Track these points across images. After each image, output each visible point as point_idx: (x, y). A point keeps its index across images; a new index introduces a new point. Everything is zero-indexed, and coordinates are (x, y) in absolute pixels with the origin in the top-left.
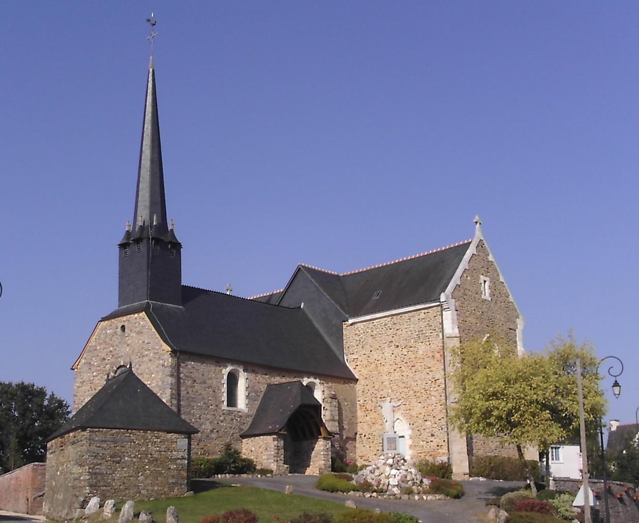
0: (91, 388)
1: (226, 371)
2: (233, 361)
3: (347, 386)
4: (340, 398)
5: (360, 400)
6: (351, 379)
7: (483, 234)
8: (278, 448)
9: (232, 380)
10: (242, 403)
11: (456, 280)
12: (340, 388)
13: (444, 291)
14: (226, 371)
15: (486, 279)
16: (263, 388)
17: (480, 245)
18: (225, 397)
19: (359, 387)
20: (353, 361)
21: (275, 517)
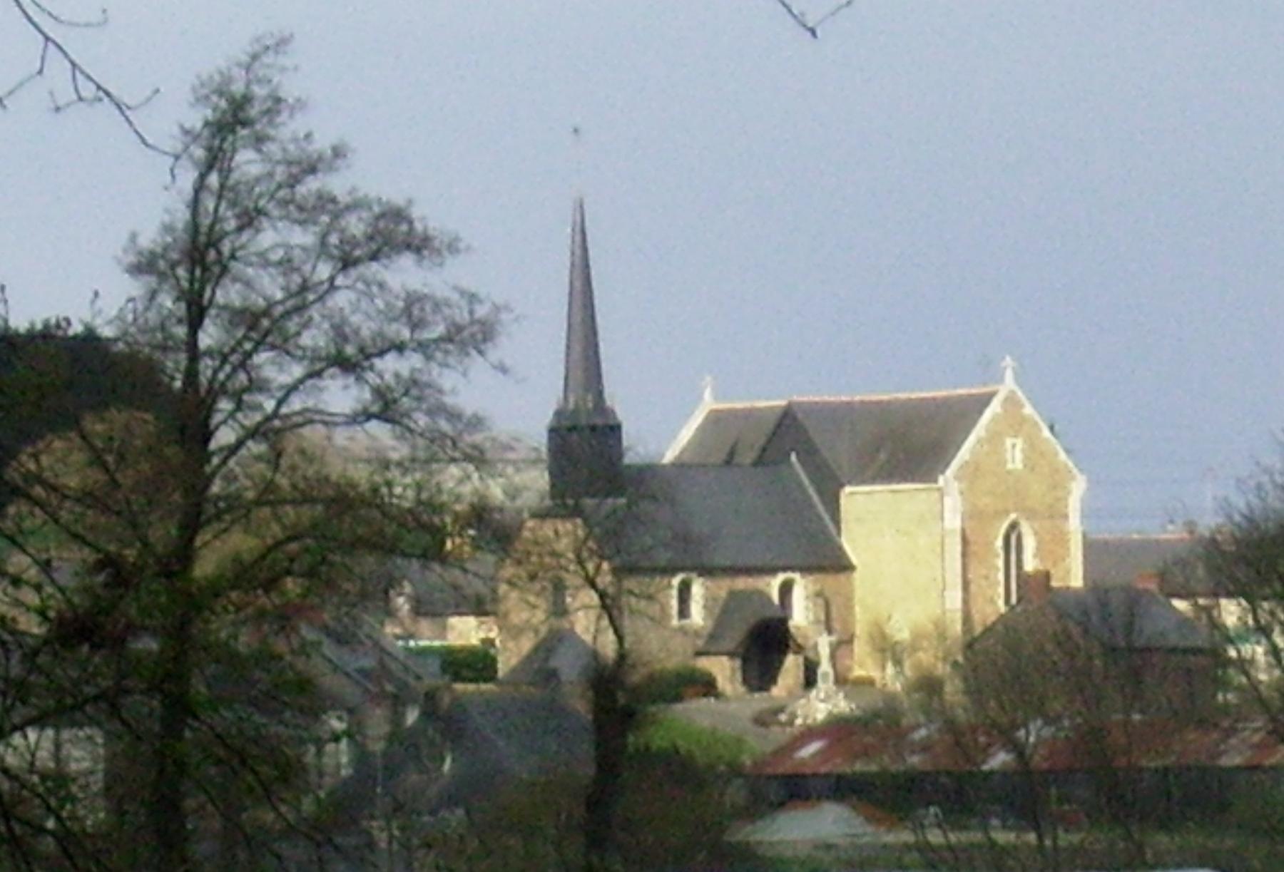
0: (79, 372)
1: (676, 581)
2: (682, 569)
3: (842, 577)
4: (827, 593)
5: (858, 594)
6: (842, 566)
7: (1018, 379)
8: (733, 670)
9: (685, 590)
10: (697, 615)
11: (964, 453)
12: (830, 582)
13: (943, 472)
14: (676, 581)
15: (1014, 440)
16: (723, 594)
17: (1011, 400)
18: (674, 603)
19: (857, 575)
20: (851, 544)
21: (304, 287)
